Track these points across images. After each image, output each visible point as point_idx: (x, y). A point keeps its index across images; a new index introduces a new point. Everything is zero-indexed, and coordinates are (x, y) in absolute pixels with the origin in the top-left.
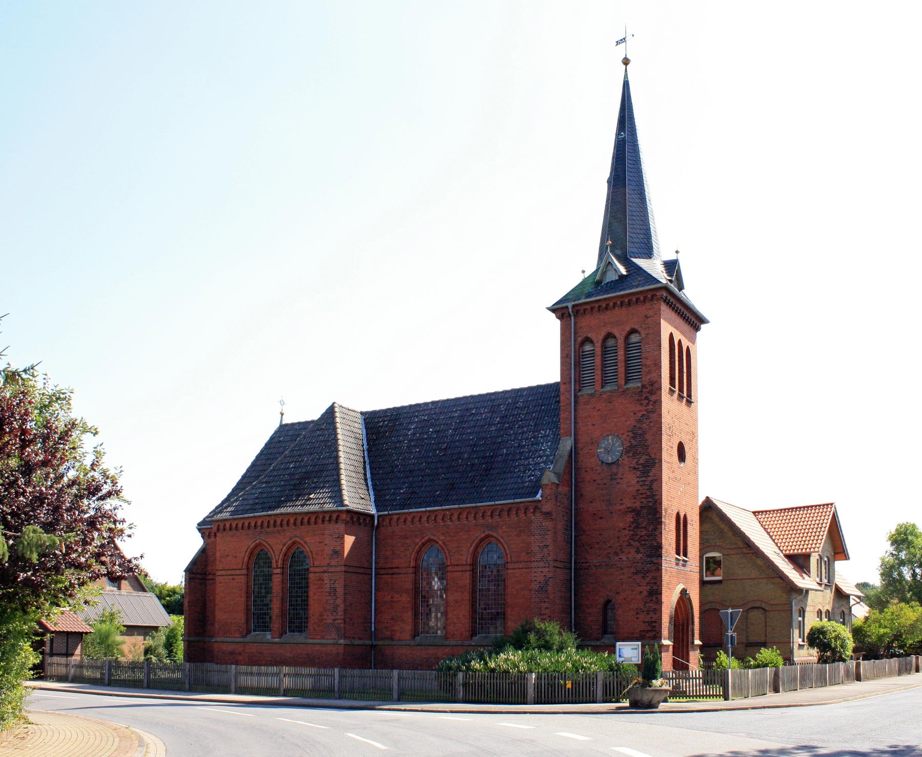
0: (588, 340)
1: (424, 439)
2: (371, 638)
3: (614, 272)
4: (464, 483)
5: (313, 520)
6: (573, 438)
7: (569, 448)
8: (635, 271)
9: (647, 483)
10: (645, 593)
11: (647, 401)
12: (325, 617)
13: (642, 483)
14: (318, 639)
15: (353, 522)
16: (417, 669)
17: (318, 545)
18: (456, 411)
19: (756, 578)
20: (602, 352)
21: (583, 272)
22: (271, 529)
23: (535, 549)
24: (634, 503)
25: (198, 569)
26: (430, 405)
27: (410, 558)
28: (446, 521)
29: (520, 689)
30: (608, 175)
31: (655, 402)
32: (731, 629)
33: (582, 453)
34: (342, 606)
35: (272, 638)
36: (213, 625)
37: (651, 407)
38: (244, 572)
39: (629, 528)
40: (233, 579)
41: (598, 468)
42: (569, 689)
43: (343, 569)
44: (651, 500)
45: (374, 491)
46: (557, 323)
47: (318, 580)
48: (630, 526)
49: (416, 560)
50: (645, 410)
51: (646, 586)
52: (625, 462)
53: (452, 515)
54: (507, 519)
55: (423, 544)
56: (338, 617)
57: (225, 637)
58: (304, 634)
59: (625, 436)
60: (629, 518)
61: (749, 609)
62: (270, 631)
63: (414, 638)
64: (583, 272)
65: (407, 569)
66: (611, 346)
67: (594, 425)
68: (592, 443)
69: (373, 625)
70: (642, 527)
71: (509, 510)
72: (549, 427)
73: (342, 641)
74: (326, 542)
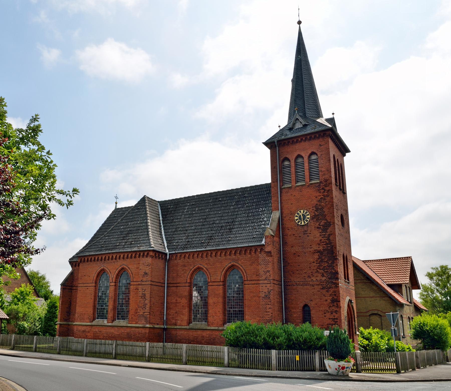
0: (287, 159)
1: (193, 214)
2: (164, 324)
3: (300, 123)
4: (218, 236)
5: (134, 255)
6: (280, 211)
7: (278, 217)
8: (312, 122)
9: (326, 236)
10: (329, 301)
11: (323, 190)
12: (139, 311)
13: (323, 236)
14: (134, 324)
15: (156, 257)
16: (190, 343)
17: (136, 269)
18: (210, 199)
19: (374, 297)
20: (295, 165)
21: (279, 126)
22: (110, 261)
23: (261, 272)
24: (319, 247)
25: (68, 283)
26: (196, 197)
27: (187, 278)
28: (208, 257)
29: (303, 360)
30: (292, 78)
31: (328, 191)
32: (394, 326)
33: (285, 219)
34: (149, 304)
35: (107, 323)
36: (74, 315)
37: (326, 193)
38: (94, 284)
39: (316, 262)
40: (87, 289)
41: (295, 228)
42: (298, 361)
43: (150, 283)
44: (329, 245)
45: (166, 241)
46: (268, 151)
47: (136, 289)
48: (317, 261)
49: (191, 279)
50: (323, 195)
51: (329, 296)
52: (312, 224)
53: (212, 253)
54: (244, 256)
55: (195, 270)
56: (146, 311)
57: (81, 322)
58: (126, 321)
59: (311, 210)
60: (316, 256)
61: (370, 315)
62: (106, 318)
63: (189, 325)
64: (279, 126)
65: (186, 284)
66: (300, 162)
67: (292, 204)
68: (291, 214)
69: (165, 316)
70: (325, 262)
71: (246, 251)
72: (264, 206)
73: (148, 326)
74: (141, 268)
